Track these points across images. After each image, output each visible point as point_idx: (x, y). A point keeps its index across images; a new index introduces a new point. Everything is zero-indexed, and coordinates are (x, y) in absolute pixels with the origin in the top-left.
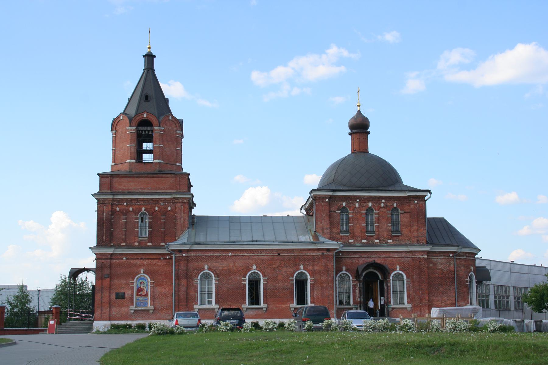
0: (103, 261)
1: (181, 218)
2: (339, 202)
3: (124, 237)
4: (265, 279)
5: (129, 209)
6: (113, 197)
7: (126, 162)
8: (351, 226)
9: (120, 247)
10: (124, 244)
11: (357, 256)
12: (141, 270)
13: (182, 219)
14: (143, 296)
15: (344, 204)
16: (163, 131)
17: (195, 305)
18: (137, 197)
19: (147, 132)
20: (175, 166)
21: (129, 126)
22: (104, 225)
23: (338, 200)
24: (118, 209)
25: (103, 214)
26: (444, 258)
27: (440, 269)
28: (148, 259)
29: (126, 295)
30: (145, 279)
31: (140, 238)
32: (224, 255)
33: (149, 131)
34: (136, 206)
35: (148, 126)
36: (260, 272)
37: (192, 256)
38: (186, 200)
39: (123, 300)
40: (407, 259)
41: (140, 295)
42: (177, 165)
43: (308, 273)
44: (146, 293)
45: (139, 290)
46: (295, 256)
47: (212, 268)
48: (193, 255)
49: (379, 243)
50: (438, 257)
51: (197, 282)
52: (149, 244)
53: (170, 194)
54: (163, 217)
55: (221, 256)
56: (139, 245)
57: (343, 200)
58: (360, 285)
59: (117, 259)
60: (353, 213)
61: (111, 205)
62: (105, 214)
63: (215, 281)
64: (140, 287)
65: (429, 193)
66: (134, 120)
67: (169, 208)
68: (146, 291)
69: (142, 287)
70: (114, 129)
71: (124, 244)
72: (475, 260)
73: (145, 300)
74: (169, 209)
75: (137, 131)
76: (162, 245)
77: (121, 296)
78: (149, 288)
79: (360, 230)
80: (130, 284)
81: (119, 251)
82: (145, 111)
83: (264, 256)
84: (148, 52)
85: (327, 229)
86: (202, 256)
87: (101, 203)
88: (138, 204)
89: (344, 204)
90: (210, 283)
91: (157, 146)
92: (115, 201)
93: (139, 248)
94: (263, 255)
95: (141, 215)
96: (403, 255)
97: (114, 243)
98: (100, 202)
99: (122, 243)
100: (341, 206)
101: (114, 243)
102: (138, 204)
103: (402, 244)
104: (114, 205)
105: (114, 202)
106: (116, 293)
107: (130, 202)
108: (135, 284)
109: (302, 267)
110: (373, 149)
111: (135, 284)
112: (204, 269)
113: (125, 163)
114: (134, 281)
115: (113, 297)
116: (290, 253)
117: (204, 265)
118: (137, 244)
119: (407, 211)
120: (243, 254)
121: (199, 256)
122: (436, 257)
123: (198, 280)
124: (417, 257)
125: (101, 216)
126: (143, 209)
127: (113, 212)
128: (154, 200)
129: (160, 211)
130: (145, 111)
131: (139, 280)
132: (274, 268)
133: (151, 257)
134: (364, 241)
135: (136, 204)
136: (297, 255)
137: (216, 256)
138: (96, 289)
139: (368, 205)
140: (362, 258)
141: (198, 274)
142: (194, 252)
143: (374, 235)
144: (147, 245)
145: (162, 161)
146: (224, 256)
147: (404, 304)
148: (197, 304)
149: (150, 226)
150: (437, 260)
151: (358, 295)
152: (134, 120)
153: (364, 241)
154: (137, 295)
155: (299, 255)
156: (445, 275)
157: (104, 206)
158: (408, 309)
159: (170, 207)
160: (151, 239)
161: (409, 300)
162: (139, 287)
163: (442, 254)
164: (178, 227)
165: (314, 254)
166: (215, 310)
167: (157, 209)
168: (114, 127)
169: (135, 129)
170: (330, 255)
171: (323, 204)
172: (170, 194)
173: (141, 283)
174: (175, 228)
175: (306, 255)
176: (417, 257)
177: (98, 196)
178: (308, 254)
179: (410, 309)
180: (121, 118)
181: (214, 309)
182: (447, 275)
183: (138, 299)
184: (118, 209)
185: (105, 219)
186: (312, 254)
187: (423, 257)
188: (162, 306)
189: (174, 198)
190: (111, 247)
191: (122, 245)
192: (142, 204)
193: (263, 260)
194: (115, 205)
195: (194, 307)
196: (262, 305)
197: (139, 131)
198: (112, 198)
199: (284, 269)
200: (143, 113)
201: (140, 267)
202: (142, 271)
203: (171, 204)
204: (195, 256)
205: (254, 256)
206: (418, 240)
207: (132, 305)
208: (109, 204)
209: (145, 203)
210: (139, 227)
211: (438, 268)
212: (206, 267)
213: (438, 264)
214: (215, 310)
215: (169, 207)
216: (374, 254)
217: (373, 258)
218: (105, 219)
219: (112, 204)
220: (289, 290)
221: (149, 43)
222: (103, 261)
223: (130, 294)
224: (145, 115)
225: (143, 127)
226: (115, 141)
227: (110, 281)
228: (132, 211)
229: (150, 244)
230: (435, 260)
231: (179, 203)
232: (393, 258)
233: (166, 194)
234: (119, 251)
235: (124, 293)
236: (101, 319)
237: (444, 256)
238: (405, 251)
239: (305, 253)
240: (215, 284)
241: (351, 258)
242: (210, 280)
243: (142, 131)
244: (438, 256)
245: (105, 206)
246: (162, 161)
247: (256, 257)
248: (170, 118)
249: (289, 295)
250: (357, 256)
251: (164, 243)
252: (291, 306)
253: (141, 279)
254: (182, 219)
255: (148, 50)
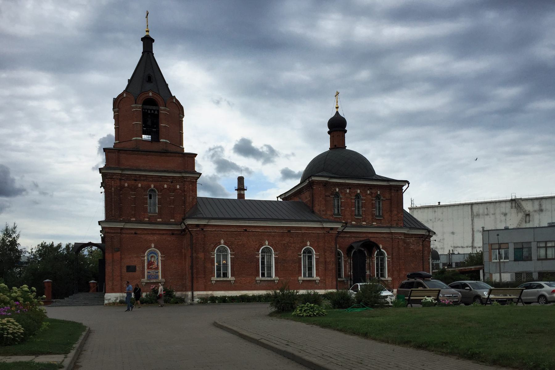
0: (112, 235)
1: (189, 196)
2: (333, 188)
3: (133, 212)
4: (276, 254)
5: (138, 185)
6: (122, 172)
7: (132, 139)
8: (343, 209)
9: (129, 222)
10: (134, 219)
11: (348, 236)
12: (152, 245)
13: (191, 198)
14: (154, 269)
15: (337, 190)
16: (168, 111)
17: (212, 278)
18: (146, 174)
19: (153, 112)
20: (179, 148)
21: (135, 103)
22: (113, 200)
23: (331, 186)
24: (126, 185)
25: (111, 189)
26: (414, 240)
27: (412, 248)
28: (159, 234)
29: (137, 269)
30: (156, 254)
31: (150, 214)
32: (238, 230)
33: (154, 111)
34: (145, 183)
35: (153, 105)
36: (272, 247)
37: (208, 231)
38: (195, 179)
39: (134, 273)
40: (388, 239)
41: (151, 269)
42: (180, 147)
43: (314, 249)
44: (156, 266)
45: (150, 264)
46: (303, 233)
47: (228, 243)
48: (209, 230)
49: (366, 225)
50: (411, 239)
51: (214, 255)
52: (158, 220)
53: (179, 173)
54: (172, 194)
55: (236, 231)
56: (149, 220)
57: (336, 187)
58: (350, 261)
59: (127, 234)
60: (344, 198)
61: (119, 180)
62: (113, 189)
63: (231, 255)
64: (151, 260)
65: (407, 184)
66: (139, 98)
67: (177, 186)
68: (156, 265)
69: (152, 261)
70: (117, 107)
71: (134, 219)
72: (431, 242)
73: (156, 273)
74: (178, 187)
75: (143, 109)
76: (172, 222)
77: (131, 269)
78: (160, 261)
79: (350, 213)
80: (141, 257)
81: (128, 226)
82: (151, 90)
83: (275, 232)
84: (147, 35)
85: (323, 211)
86: (218, 231)
87: (109, 178)
88: (147, 181)
89: (337, 190)
90: (225, 258)
91: (163, 126)
92: (123, 177)
93: (150, 223)
94: (275, 231)
95: (149, 191)
96: (384, 236)
97: (124, 218)
98: (108, 177)
99: (131, 218)
100: (335, 191)
101: (124, 218)
102: (147, 181)
103: (384, 226)
104: (123, 181)
105: (123, 177)
106: (127, 266)
107: (137, 178)
108: (146, 258)
109: (308, 243)
110: (350, 146)
111: (146, 258)
112: (220, 243)
113: (132, 140)
114: (144, 255)
115: (124, 270)
116: (298, 231)
117: (220, 240)
118: (147, 219)
119: (388, 198)
120: (256, 230)
121: (215, 231)
122: (409, 239)
123: (215, 253)
124: (396, 237)
125: (110, 191)
126: (152, 186)
127: (122, 187)
128: (162, 177)
129: (168, 189)
130: (151, 90)
131: (150, 254)
132: (284, 244)
133: (161, 232)
134: (353, 223)
135: (145, 181)
136: (304, 233)
137: (231, 231)
138: (106, 262)
139: (357, 191)
140: (352, 237)
141: (214, 248)
142: (210, 226)
143: (361, 218)
144: (157, 221)
145: (168, 141)
146: (239, 231)
147: (385, 277)
148: (215, 277)
149: (159, 203)
150: (410, 241)
151: (348, 269)
152: (139, 98)
153: (353, 223)
154: (148, 268)
155: (306, 233)
156: (415, 253)
157: (112, 181)
158: (276, 282)
159: (179, 185)
160: (160, 215)
161: (389, 274)
162: (150, 260)
163: (413, 236)
164: (187, 205)
165: (319, 232)
166: (317, 281)
167: (166, 186)
168: (117, 105)
169: (141, 107)
170: (333, 233)
171: (319, 189)
172: (180, 173)
173: (152, 257)
174: (185, 206)
175: (312, 233)
176: (396, 237)
177: (106, 171)
178: (314, 232)
179: (390, 281)
180: (125, 95)
181: (231, 281)
182: (417, 254)
183: (149, 272)
184: (126, 185)
185: (113, 194)
186: (317, 232)
187: (401, 238)
188: (173, 279)
189: (183, 177)
190: (120, 221)
191: (131, 220)
192: (151, 181)
193: (274, 236)
194: (124, 181)
195: (212, 279)
196: (230, 277)
197: (145, 109)
198: (121, 174)
199: (293, 245)
200: (149, 92)
201: (151, 242)
202: (153, 245)
203: (179, 182)
204: (212, 231)
205: (266, 232)
206: (397, 224)
207: (144, 278)
208: (118, 179)
209: (154, 180)
210: (148, 204)
211: (410, 247)
212: (222, 241)
213: (411, 244)
214: (231, 282)
215: (178, 185)
216: (361, 234)
217: (361, 237)
218: (113, 194)
219: (120, 180)
220: (297, 264)
221: (147, 26)
222: (112, 235)
223: (141, 267)
224: (151, 94)
225: (149, 106)
226: (118, 120)
227: (121, 255)
228: (141, 188)
229: (160, 220)
230: (408, 241)
231: (188, 181)
232: (377, 238)
233: (175, 172)
234: (128, 226)
235: (136, 266)
236: (113, 291)
237: (415, 237)
238: (386, 232)
239: (311, 231)
240: (231, 258)
241: (343, 237)
242: (225, 253)
243: (148, 110)
244: (410, 238)
245: (113, 181)
246: (168, 141)
247: (268, 233)
248: (174, 101)
249: (297, 268)
250: (348, 236)
251: (174, 219)
252: (300, 278)
253: (151, 253)
254: (191, 198)
255: (147, 33)
